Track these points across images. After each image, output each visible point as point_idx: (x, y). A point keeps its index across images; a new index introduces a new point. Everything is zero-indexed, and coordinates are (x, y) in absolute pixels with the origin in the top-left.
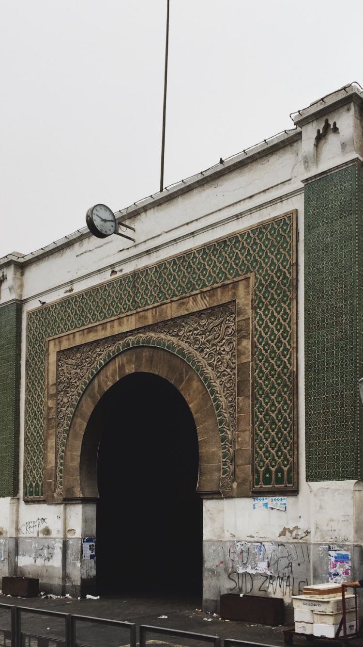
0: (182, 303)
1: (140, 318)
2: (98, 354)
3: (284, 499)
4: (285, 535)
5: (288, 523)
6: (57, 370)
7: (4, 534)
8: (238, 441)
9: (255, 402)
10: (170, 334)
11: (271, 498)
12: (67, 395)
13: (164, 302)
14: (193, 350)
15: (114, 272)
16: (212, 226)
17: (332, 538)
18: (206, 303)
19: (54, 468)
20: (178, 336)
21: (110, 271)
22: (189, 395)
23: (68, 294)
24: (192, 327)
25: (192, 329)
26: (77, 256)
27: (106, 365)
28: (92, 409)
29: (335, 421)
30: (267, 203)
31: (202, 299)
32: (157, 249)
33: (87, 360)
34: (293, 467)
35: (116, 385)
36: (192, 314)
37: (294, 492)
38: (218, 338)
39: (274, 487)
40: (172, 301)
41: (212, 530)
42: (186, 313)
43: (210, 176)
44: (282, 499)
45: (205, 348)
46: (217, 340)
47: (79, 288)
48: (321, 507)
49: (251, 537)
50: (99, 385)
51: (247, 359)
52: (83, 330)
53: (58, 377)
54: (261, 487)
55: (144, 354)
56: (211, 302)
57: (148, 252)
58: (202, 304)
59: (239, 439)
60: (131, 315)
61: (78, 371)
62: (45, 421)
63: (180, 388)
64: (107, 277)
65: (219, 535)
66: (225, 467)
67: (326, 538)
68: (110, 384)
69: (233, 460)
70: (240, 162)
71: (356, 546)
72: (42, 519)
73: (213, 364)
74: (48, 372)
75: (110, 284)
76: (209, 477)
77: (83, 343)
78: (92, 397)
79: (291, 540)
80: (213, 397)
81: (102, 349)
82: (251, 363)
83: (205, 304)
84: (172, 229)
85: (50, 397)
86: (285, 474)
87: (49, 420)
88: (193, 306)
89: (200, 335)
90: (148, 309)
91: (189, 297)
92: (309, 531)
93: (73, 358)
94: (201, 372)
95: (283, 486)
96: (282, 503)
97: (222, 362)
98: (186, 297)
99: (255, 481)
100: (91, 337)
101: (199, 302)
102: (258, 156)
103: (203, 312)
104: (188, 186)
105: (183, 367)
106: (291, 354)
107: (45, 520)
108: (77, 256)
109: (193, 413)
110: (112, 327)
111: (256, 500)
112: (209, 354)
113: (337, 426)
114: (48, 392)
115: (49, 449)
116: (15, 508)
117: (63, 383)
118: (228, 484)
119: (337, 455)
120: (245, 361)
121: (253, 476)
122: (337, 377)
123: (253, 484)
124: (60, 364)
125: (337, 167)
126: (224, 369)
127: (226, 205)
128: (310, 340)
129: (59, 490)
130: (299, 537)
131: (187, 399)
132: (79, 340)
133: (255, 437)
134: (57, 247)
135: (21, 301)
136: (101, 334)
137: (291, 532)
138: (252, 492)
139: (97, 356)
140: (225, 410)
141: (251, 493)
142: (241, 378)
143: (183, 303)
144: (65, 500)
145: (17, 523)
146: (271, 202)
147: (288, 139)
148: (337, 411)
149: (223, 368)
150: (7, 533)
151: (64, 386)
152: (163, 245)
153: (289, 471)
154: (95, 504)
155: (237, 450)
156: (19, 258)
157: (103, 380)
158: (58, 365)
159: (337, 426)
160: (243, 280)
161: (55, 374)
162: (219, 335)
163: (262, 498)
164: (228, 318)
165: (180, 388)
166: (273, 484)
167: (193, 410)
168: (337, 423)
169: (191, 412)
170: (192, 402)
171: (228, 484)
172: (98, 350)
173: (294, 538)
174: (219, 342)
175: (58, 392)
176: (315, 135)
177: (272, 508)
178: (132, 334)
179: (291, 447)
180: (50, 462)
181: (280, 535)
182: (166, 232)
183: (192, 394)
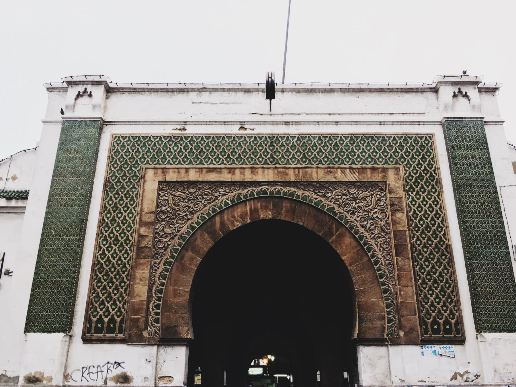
0: (329, 170)
1: (279, 173)
2: (220, 193)
3: (452, 347)
4: (456, 379)
5: (458, 369)
6: (158, 198)
7: (45, 382)
8: (400, 295)
9: (416, 263)
10: (315, 193)
11: (439, 346)
12: (171, 226)
14: (343, 211)
15: (242, 128)
16: (356, 123)
17: (509, 380)
18: (356, 177)
19: (145, 303)
20: (325, 196)
21: (239, 126)
24: (340, 192)
25: (340, 194)
26: (193, 103)
28: (211, 245)
29: (498, 287)
30: (269, 122)
31: (352, 174)
32: (297, 123)
33: (205, 196)
34: (459, 320)
35: (244, 227)
36: (340, 182)
37: (462, 341)
38: (369, 206)
39: (456, 336)
40: (318, 168)
41: (374, 376)
42: (334, 180)
43: (354, 89)
44: (450, 348)
45: (356, 212)
46: (370, 207)
47: (191, 130)
48: (496, 354)
49: (422, 381)
50: (222, 223)
51: (403, 226)
52: (202, 168)
54: (430, 336)
55: (284, 205)
56: (360, 177)
58: (350, 177)
59: (402, 293)
60: (269, 168)
62: (134, 249)
63: (330, 241)
64: (235, 130)
65: (382, 381)
66: (390, 316)
67: (504, 380)
69: (397, 311)
70: (381, 89)
72: (116, 363)
73: (366, 226)
74: (142, 200)
75: (234, 138)
76: (370, 325)
77: (200, 180)
79: (463, 383)
80: (371, 253)
81: (228, 191)
82: (408, 232)
83: (355, 178)
84: (314, 113)
86: (453, 326)
88: (339, 176)
89: (350, 200)
90: (289, 168)
91: (337, 168)
92: (478, 374)
93: (184, 192)
94: (355, 231)
95: (453, 336)
96: (451, 351)
97: (375, 227)
98: (333, 168)
99: (423, 330)
100: (212, 177)
101: (348, 174)
102: (396, 90)
103: (353, 183)
104: (331, 89)
105: (332, 223)
106: (445, 231)
107: (121, 365)
108: (193, 103)
109: (347, 265)
110: (242, 173)
111: (424, 348)
112: (361, 218)
113: (500, 290)
114: (140, 219)
115: (138, 281)
116: (66, 347)
117: (166, 213)
118: (395, 332)
119: (504, 312)
120: (402, 229)
121: (421, 326)
122: (494, 255)
123: (421, 333)
124: (162, 194)
125: (471, 118)
126: (378, 232)
127: (369, 113)
128: (466, 224)
129: (153, 329)
130: (470, 380)
131: (339, 251)
132: (193, 176)
133: (419, 292)
134: (167, 89)
136: (226, 177)
137: (462, 376)
138: (421, 340)
140: (384, 266)
141: (420, 341)
142: (399, 242)
143: (331, 172)
146: (411, 122)
147: (421, 88)
148: (498, 279)
149: (377, 231)
150: (50, 379)
151: (167, 217)
152: (304, 122)
153: (457, 323)
154: (183, 345)
155: (401, 302)
157: (228, 219)
158: (159, 194)
159: (500, 290)
160: (393, 168)
161: (155, 203)
162: (371, 204)
163: (430, 346)
164: (378, 193)
165: (330, 241)
166: (454, 334)
168: (500, 288)
169: (345, 264)
170: (345, 255)
171: (395, 332)
172: (221, 190)
173: (466, 381)
174: (371, 210)
176: (77, 93)
177: (441, 355)
179: (455, 304)
180: (137, 295)
181: (452, 379)
182: (307, 114)
183: (344, 247)
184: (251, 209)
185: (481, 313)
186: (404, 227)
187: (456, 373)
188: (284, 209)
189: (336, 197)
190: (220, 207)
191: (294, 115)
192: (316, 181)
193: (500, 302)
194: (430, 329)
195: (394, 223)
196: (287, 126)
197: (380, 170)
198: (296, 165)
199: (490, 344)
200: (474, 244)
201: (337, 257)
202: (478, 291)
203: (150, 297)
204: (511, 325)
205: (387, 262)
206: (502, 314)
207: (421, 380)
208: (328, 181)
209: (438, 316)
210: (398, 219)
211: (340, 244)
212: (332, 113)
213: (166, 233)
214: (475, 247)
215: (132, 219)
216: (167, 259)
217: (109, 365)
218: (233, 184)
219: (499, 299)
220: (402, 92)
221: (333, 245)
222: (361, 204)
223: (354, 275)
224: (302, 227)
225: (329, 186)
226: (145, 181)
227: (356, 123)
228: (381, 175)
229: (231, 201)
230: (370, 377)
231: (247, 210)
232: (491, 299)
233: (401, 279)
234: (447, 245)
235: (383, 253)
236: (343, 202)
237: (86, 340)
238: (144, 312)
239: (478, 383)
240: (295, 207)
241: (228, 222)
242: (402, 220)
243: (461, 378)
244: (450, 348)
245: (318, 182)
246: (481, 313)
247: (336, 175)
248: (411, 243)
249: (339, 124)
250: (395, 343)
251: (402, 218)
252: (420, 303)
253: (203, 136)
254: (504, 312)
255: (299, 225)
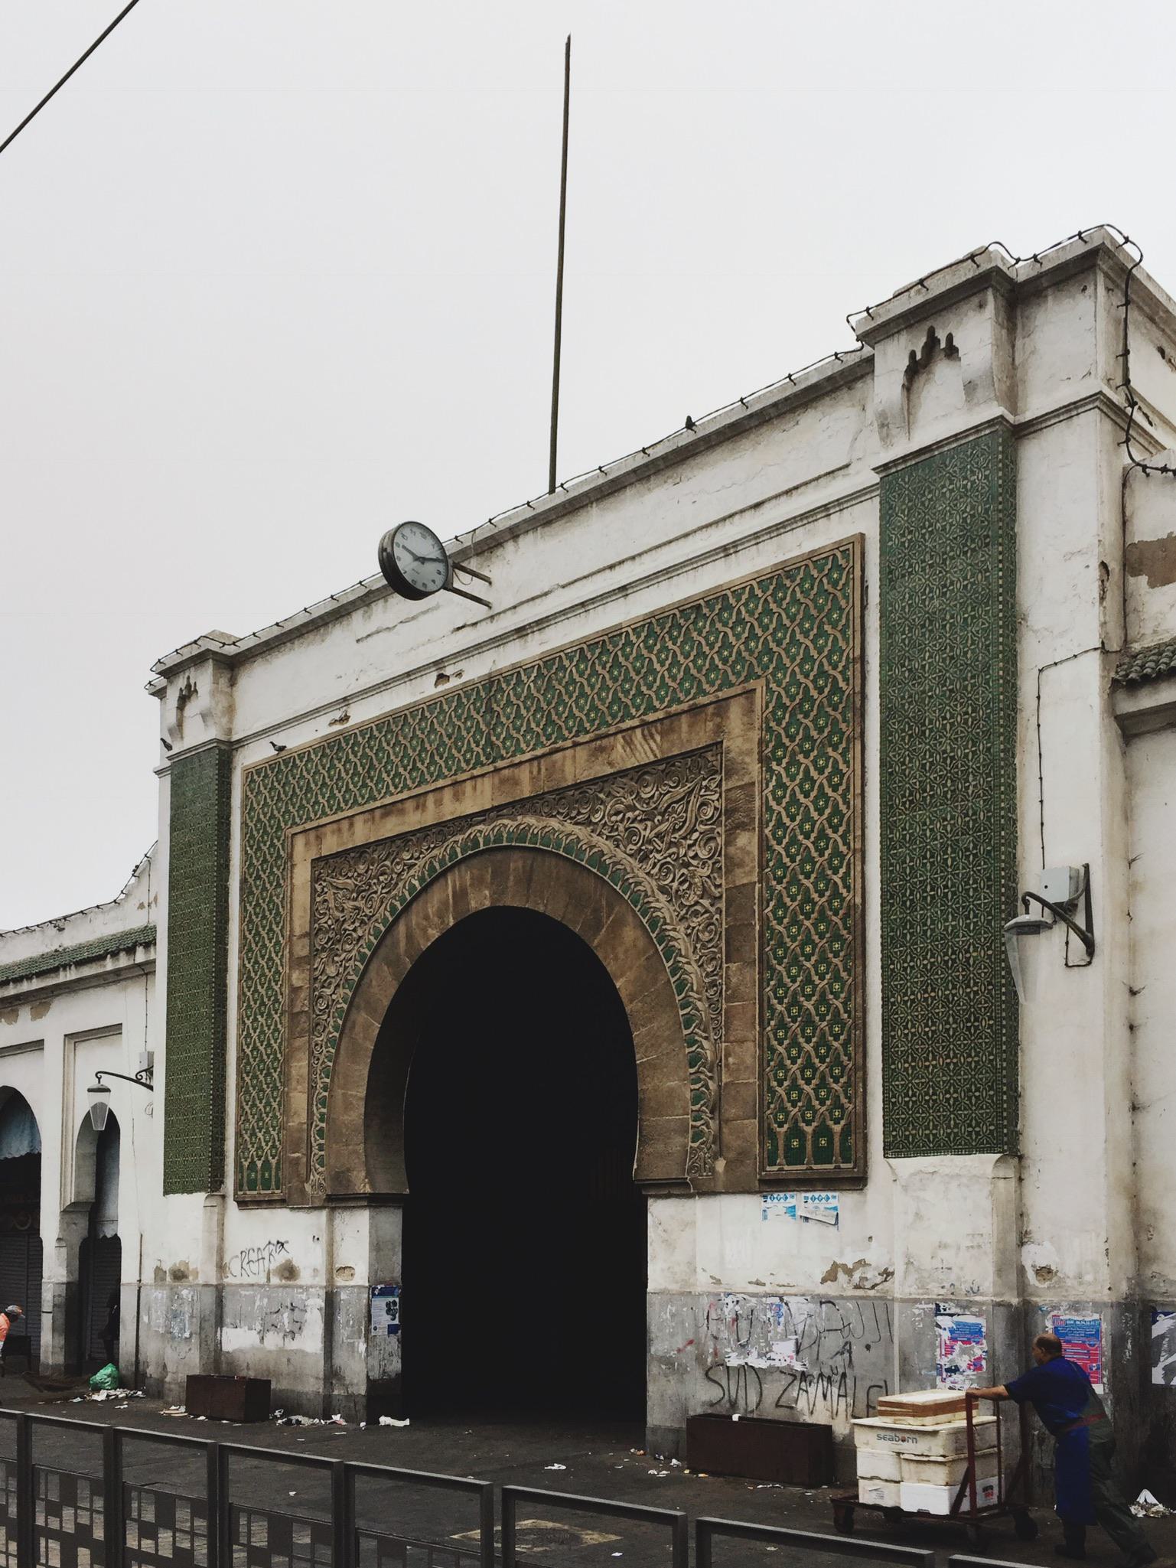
0: (599, 747)
2: (405, 865)
3: (834, 1197)
4: (835, 1279)
5: (842, 1254)
8: (727, 1065)
11: (804, 1194)
12: (336, 959)
13: (557, 746)
15: (442, 678)
16: (668, 572)
18: (655, 747)
19: (305, 1126)
20: (590, 823)
21: (433, 676)
22: (616, 958)
23: (338, 727)
24: (622, 803)
25: (621, 807)
26: (358, 641)
27: (415, 899)
31: (646, 740)
32: (541, 624)
33: (381, 878)
36: (623, 773)
37: (857, 1181)
39: (811, 1169)
40: (576, 745)
42: (609, 770)
43: (664, 458)
45: (651, 852)
47: (362, 713)
48: (918, 1216)
49: (758, 1283)
50: (410, 937)
52: (372, 810)
53: (314, 920)
56: (665, 746)
57: (521, 632)
58: (644, 752)
59: (731, 1060)
61: (360, 903)
62: (286, 1019)
64: (426, 688)
66: (698, 1123)
68: (434, 934)
71: (999, 1304)
73: (671, 887)
75: (432, 704)
76: (660, 1147)
78: (393, 963)
81: (416, 855)
82: (758, 886)
83: (652, 751)
85: (297, 962)
86: (837, 1139)
87: (294, 1017)
88: (623, 757)
89: (641, 821)
92: (890, 1270)
93: (350, 875)
97: (691, 884)
98: (608, 736)
100: (392, 827)
101: (638, 746)
106: (848, 864)
108: (358, 641)
109: (625, 1000)
110: (439, 803)
114: (291, 952)
115: (294, 1083)
119: (955, 1095)
120: (745, 881)
124: (319, 888)
125: (956, 437)
126: (696, 898)
128: (891, 833)
129: (317, 1176)
130: (868, 1285)
132: (362, 833)
135: (231, 743)
136: (413, 820)
137: (849, 1272)
139: (403, 870)
140: (697, 993)
142: (736, 920)
144: (330, 1198)
145: (221, 1251)
147: (842, 372)
148: (954, 995)
151: (329, 939)
152: (555, 615)
153: (846, 1133)
154: (399, 1208)
155: (726, 1084)
156: (224, 644)
157: (418, 924)
158: (314, 891)
163: (782, 1195)
167: (623, 994)
168: (955, 1022)
170: (622, 976)
172: (406, 856)
173: (857, 1287)
174: (685, 838)
175: (315, 953)
177: (807, 1219)
178: (484, 820)
180: (295, 1113)
181: (824, 1281)
182: (563, 587)
183: (621, 956)
184: (454, 892)
185: (893, 1100)
186: (751, 872)
187: (835, 1266)
188: (512, 878)
189: (614, 818)
190: (402, 899)
191: (538, 601)
192: (572, 786)
193: (948, 1064)
194: (781, 1152)
195: (732, 864)
196: (522, 641)
197: (711, 709)
198: (532, 750)
199: (905, 1188)
200: (904, 895)
201: (606, 981)
202: (893, 1037)
203: (310, 1114)
204: (970, 1133)
205: (707, 980)
206: (948, 1100)
207: (754, 1280)
208: (595, 779)
209: (803, 1116)
210: (739, 853)
211: (614, 949)
212: (641, 551)
213: (329, 977)
214: (904, 903)
215: (841, 830)
216: (330, 1033)
217: (271, 1247)
218: (424, 832)
219: (948, 1056)
220: (780, 416)
221: (600, 955)
222: (663, 827)
223: (636, 1025)
224: (543, 915)
225: (600, 792)
226: (293, 866)
227: (668, 572)
228: (711, 724)
229: (419, 880)
230: (663, 1270)
231: (448, 896)
232: (927, 1059)
233: (731, 1024)
234: (849, 906)
235: (701, 957)
236: (626, 830)
237: (242, 1204)
238: (304, 1145)
239: (887, 1291)
240: (532, 865)
241: (418, 931)
242: (748, 853)
243: (846, 1277)
244: (828, 1198)
245: (577, 786)
246: (893, 1100)
247: (614, 756)
248: (761, 919)
249: (629, 591)
250: (707, 1191)
251: (748, 848)
252: (765, 1083)
253: (808, 562)
254: (955, 1095)
255: (537, 912)
